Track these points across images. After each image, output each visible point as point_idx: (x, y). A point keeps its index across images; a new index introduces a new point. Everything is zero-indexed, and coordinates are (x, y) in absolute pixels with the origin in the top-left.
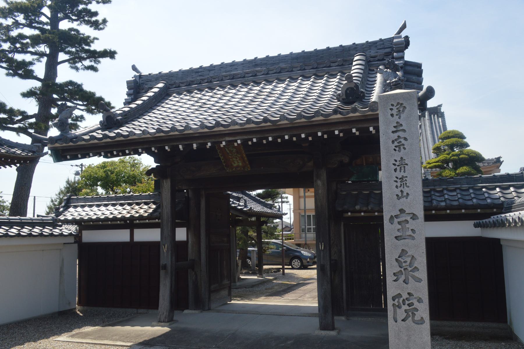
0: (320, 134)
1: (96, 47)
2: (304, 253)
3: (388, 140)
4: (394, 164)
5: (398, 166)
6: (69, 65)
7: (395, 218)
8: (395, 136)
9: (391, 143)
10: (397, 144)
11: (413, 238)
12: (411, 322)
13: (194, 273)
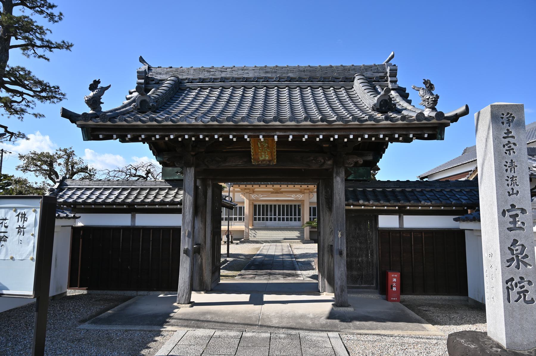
0: (216, 137)
1: (52, 37)
3: (500, 144)
4: (506, 166)
5: (509, 167)
6: (21, 51)
7: (506, 212)
8: (506, 141)
9: (502, 147)
10: (508, 149)
11: (523, 229)
12: (523, 302)
13: (200, 256)
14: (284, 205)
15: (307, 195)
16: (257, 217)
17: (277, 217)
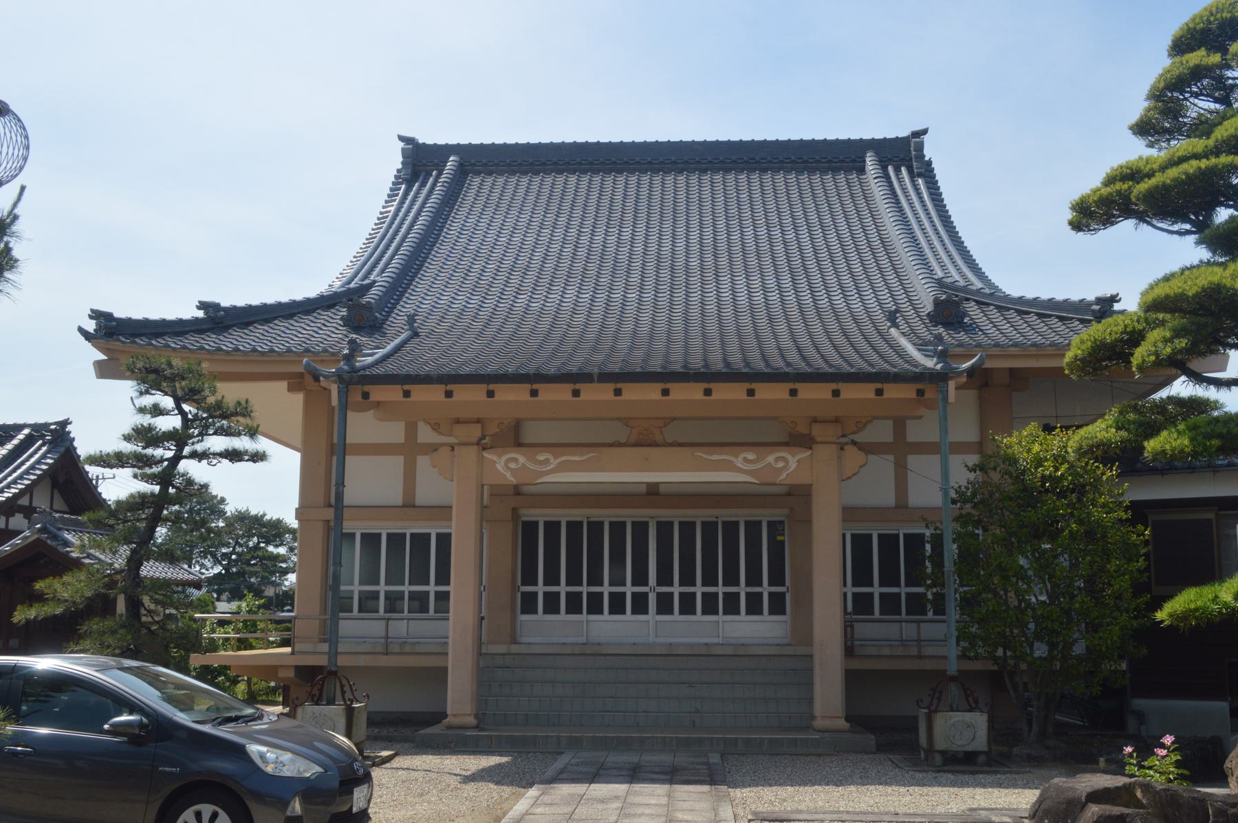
2: (271, 756)
14: (693, 524)
15: (824, 453)
16: (541, 589)
17: (652, 588)
